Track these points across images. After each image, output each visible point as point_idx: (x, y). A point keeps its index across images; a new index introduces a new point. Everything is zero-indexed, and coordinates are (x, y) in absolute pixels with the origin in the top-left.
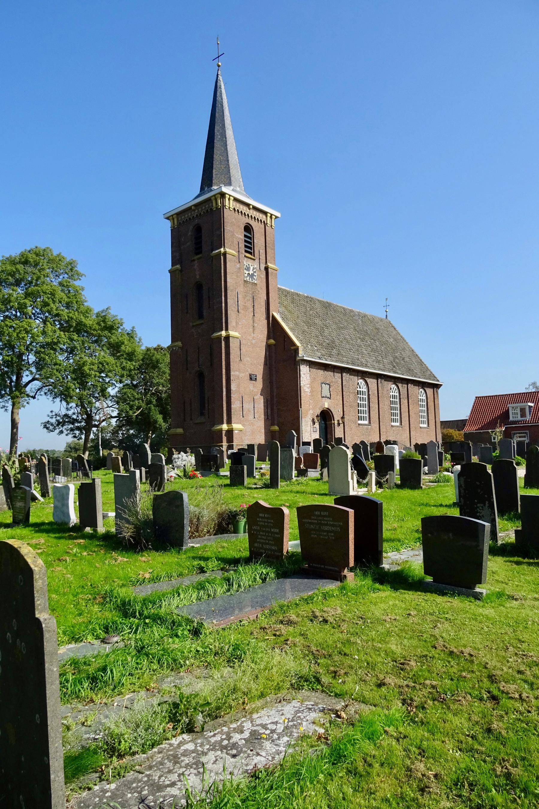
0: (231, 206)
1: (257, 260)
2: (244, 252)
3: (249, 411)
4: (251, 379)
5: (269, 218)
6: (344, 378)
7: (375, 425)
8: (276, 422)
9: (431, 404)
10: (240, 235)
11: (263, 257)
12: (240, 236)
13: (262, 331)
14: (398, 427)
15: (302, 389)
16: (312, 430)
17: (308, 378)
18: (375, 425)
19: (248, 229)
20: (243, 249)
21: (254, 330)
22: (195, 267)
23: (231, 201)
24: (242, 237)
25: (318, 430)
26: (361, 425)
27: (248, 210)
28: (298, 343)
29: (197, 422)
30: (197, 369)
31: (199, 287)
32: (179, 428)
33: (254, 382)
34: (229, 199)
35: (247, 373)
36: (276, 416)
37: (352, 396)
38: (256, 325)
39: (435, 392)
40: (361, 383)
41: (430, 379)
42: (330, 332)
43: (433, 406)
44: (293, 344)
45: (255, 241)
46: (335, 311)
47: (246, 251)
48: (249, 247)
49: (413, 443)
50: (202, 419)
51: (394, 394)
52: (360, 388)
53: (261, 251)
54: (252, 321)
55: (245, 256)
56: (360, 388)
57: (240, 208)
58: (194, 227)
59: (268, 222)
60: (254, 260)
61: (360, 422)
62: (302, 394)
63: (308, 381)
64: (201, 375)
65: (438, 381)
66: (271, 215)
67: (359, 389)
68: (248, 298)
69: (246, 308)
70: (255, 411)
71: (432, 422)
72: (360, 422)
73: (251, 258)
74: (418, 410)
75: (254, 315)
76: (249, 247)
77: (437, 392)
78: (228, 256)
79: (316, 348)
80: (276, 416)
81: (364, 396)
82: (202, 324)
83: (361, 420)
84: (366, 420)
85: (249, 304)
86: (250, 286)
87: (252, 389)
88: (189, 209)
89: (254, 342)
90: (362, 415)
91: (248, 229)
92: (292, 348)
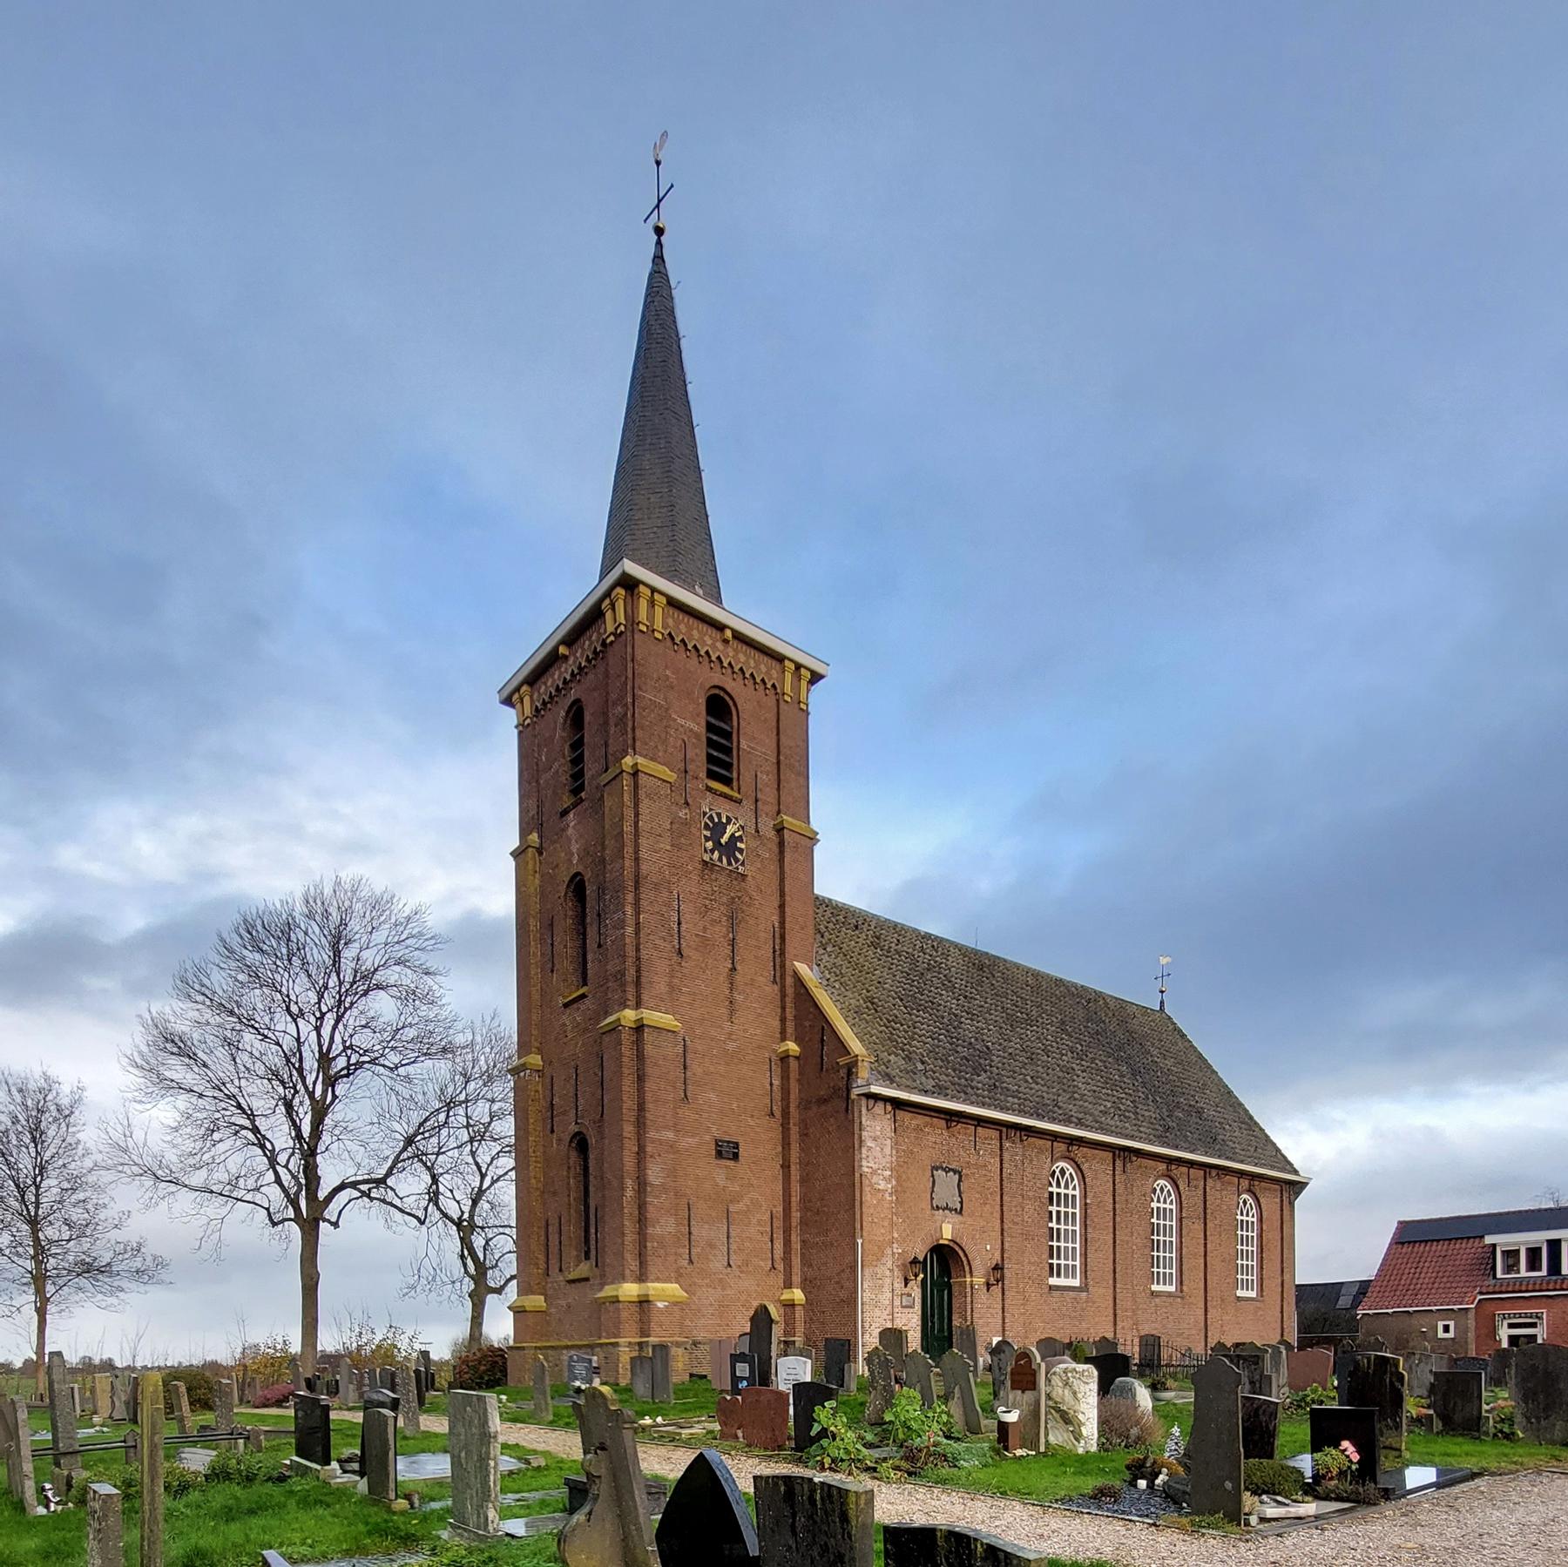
0: (658, 625)
1: (748, 804)
2: (703, 775)
3: (712, 1246)
4: (719, 1155)
5: (788, 676)
6: (1006, 1156)
7: (1101, 1292)
8: (796, 1279)
9: (1272, 1236)
10: (692, 722)
11: (768, 795)
12: (691, 725)
13: (760, 1015)
14: (1169, 1294)
15: (866, 1182)
16: (898, 1302)
17: (888, 1150)
18: (1102, 1291)
19: (719, 706)
20: (699, 766)
21: (732, 1012)
22: (570, 831)
23: (658, 611)
24: (702, 730)
25: (918, 1301)
26: (1058, 1288)
27: (719, 645)
28: (856, 1046)
29: (571, 1277)
30: (573, 1128)
31: (577, 886)
32: (533, 1293)
33: (731, 1163)
34: (652, 603)
35: (707, 1138)
36: (796, 1261)
37: (1030, 1207)
38: (739, 998)
39: (1286, 1202)
40: (1063, 1172)
41: (1272, 1168)
42: (979, 1031)
43: (1278, 1242)
44: (844, 1049)
45: (743, 745)
46: (1005, 980)
47: (712, 775)
48: (721, 761)
49: (1212, 1343)
50: (584, 1269)
51: (1162, 1205)
52: (1058, 1185)
53: (763, 777)
54: (727, 985)
55: (709, 789)
56: (1058, 1185)
57: (691, 637)
58: (568, 713)
59: (788, 689)
60: (739, 802)
61: (1053, 1281)
62: (867, 1197)
63: (888, 1159)
64: (581, 1144)
65: (1296, 1172)
66: (798, 666)
67: (1054, 1189)
68: (715, 915)
69: (705, 944)
70: (733, 1247)
71: (1273, 1285)
72: (1053, 1281)
73: (726, 796)
74: (1232, 1252)
75: (734, 969)
76: (721, 761)
77: (1292, 1204)
78: (642, 779)
79: (920, 1066)
80: (796, 1261)
81: (1070, 1210)
82: (583, 996)
83: (1059, 1275)
84: (1074, 1276)
85: (719, 932)
86: (723, 879)
87: (721, 1183)
88: (551, 660)
89: (731, 1046)
90: (1062, 1262)
91: (719, 706)
92: (842, 1061)
